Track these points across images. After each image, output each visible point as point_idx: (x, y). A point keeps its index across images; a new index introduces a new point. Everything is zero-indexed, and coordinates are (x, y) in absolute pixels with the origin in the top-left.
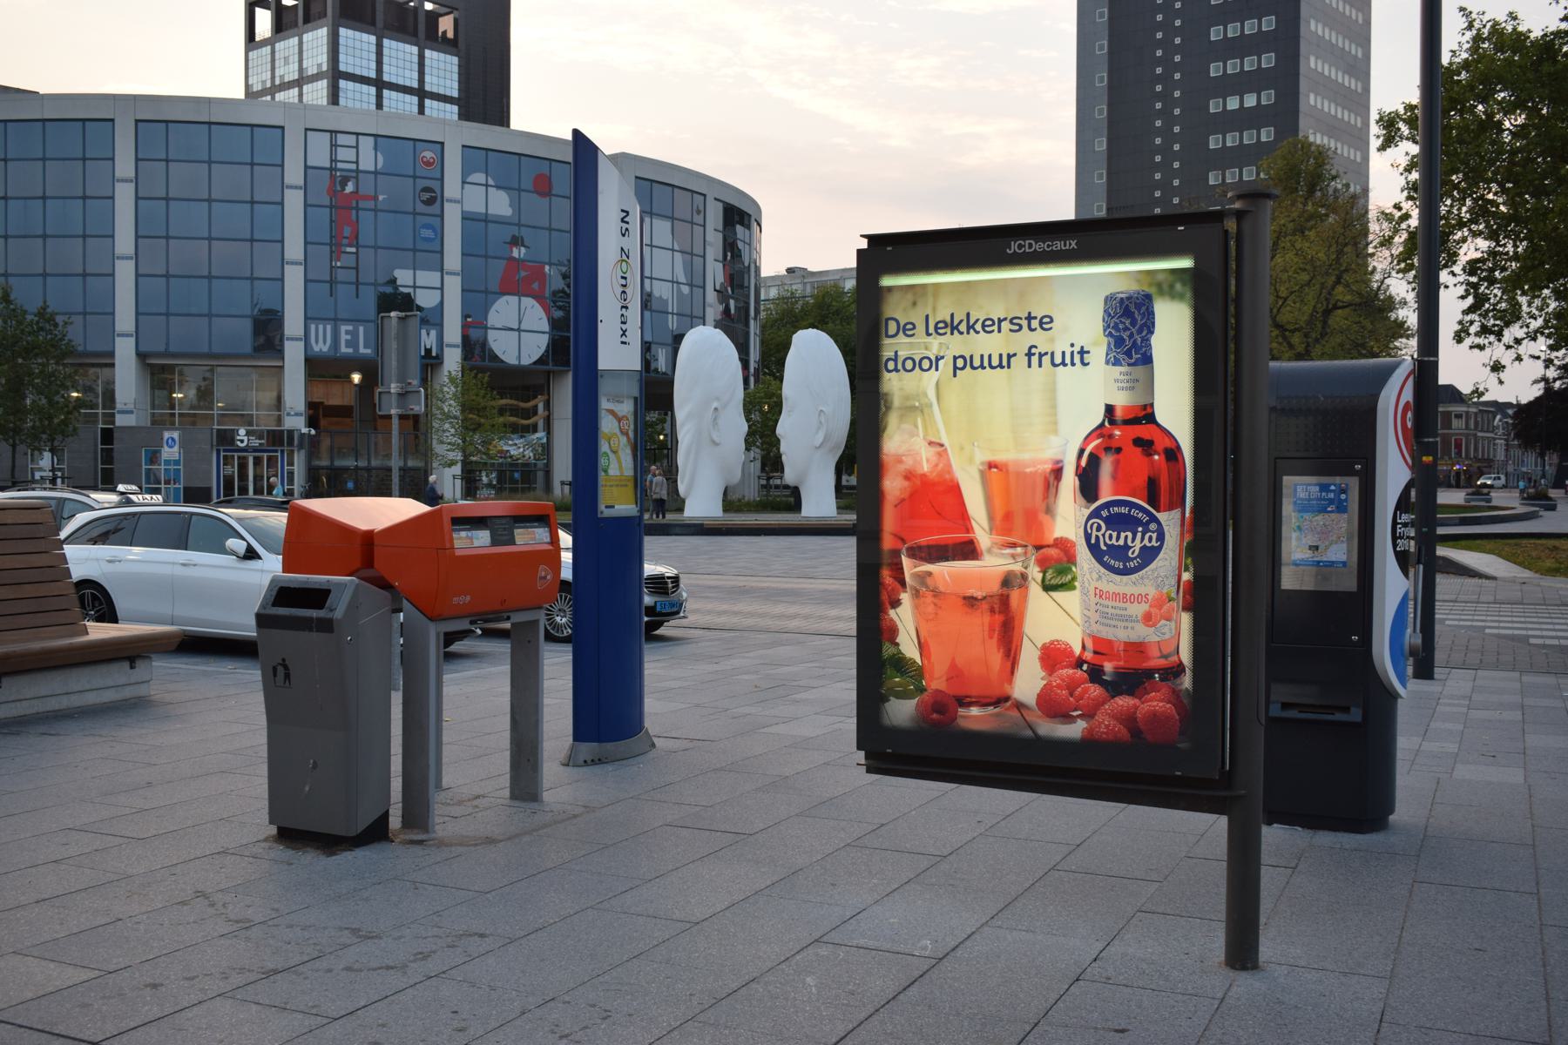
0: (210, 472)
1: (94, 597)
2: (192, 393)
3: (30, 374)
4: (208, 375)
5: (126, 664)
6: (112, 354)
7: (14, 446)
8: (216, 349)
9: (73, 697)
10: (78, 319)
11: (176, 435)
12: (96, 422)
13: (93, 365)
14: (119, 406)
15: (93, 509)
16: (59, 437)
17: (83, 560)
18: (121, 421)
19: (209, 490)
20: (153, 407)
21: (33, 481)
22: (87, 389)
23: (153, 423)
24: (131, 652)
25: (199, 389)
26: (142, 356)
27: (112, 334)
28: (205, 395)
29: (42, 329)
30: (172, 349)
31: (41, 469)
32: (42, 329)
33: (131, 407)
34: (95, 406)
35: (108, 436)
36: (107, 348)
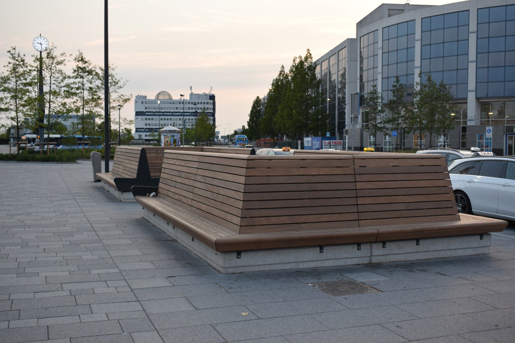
0: (503, 143)
1: (461, 197)
2: (496, 113)
3: (437, 107)
4: (503, 105)
5: (478, 237)
6: (466, 99)
7: (431, 133)
8: (506, 95)
9: (452, 252)
10: (454, 87)
11: (491, 128)
12: (460, 124)
13: (460, 103)
14: (469, 118)
15: (461, 158)
16: (447, 130)
17: (458, 181)
18: (469, 123)
19: (502, 150)
20: (481, 118)
21: (437, 146)
22: (457, 112)
23: (481, 124)
24: (480, 231)
25: (498, 111)
26: (477, 99)
27: (467, 91)
28: (501, 113)
29: (441, 91)
30: (489, 95)
31: (440, 142)
32: (441, 91)
33: (473, 118)
34: (459, 118)
35: (464, 129)
36: (465, 97)
